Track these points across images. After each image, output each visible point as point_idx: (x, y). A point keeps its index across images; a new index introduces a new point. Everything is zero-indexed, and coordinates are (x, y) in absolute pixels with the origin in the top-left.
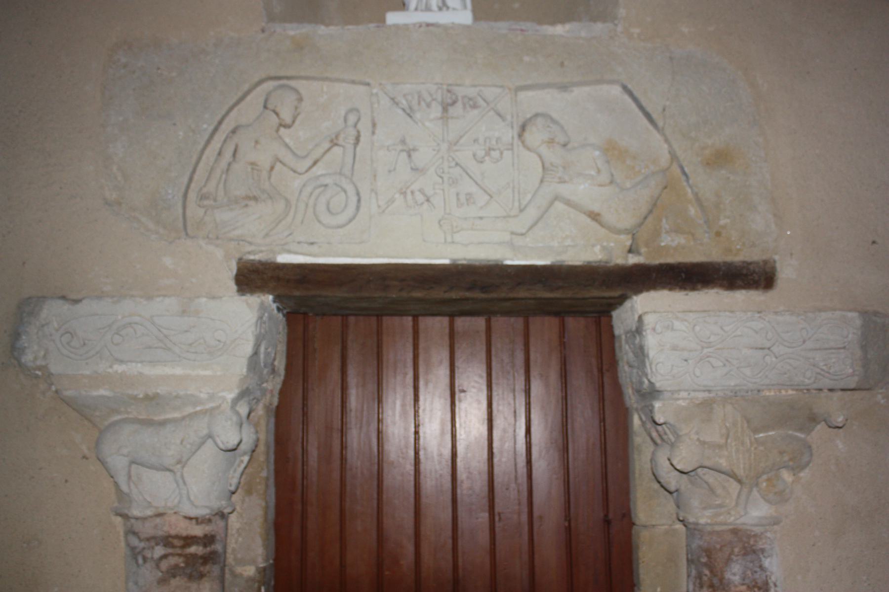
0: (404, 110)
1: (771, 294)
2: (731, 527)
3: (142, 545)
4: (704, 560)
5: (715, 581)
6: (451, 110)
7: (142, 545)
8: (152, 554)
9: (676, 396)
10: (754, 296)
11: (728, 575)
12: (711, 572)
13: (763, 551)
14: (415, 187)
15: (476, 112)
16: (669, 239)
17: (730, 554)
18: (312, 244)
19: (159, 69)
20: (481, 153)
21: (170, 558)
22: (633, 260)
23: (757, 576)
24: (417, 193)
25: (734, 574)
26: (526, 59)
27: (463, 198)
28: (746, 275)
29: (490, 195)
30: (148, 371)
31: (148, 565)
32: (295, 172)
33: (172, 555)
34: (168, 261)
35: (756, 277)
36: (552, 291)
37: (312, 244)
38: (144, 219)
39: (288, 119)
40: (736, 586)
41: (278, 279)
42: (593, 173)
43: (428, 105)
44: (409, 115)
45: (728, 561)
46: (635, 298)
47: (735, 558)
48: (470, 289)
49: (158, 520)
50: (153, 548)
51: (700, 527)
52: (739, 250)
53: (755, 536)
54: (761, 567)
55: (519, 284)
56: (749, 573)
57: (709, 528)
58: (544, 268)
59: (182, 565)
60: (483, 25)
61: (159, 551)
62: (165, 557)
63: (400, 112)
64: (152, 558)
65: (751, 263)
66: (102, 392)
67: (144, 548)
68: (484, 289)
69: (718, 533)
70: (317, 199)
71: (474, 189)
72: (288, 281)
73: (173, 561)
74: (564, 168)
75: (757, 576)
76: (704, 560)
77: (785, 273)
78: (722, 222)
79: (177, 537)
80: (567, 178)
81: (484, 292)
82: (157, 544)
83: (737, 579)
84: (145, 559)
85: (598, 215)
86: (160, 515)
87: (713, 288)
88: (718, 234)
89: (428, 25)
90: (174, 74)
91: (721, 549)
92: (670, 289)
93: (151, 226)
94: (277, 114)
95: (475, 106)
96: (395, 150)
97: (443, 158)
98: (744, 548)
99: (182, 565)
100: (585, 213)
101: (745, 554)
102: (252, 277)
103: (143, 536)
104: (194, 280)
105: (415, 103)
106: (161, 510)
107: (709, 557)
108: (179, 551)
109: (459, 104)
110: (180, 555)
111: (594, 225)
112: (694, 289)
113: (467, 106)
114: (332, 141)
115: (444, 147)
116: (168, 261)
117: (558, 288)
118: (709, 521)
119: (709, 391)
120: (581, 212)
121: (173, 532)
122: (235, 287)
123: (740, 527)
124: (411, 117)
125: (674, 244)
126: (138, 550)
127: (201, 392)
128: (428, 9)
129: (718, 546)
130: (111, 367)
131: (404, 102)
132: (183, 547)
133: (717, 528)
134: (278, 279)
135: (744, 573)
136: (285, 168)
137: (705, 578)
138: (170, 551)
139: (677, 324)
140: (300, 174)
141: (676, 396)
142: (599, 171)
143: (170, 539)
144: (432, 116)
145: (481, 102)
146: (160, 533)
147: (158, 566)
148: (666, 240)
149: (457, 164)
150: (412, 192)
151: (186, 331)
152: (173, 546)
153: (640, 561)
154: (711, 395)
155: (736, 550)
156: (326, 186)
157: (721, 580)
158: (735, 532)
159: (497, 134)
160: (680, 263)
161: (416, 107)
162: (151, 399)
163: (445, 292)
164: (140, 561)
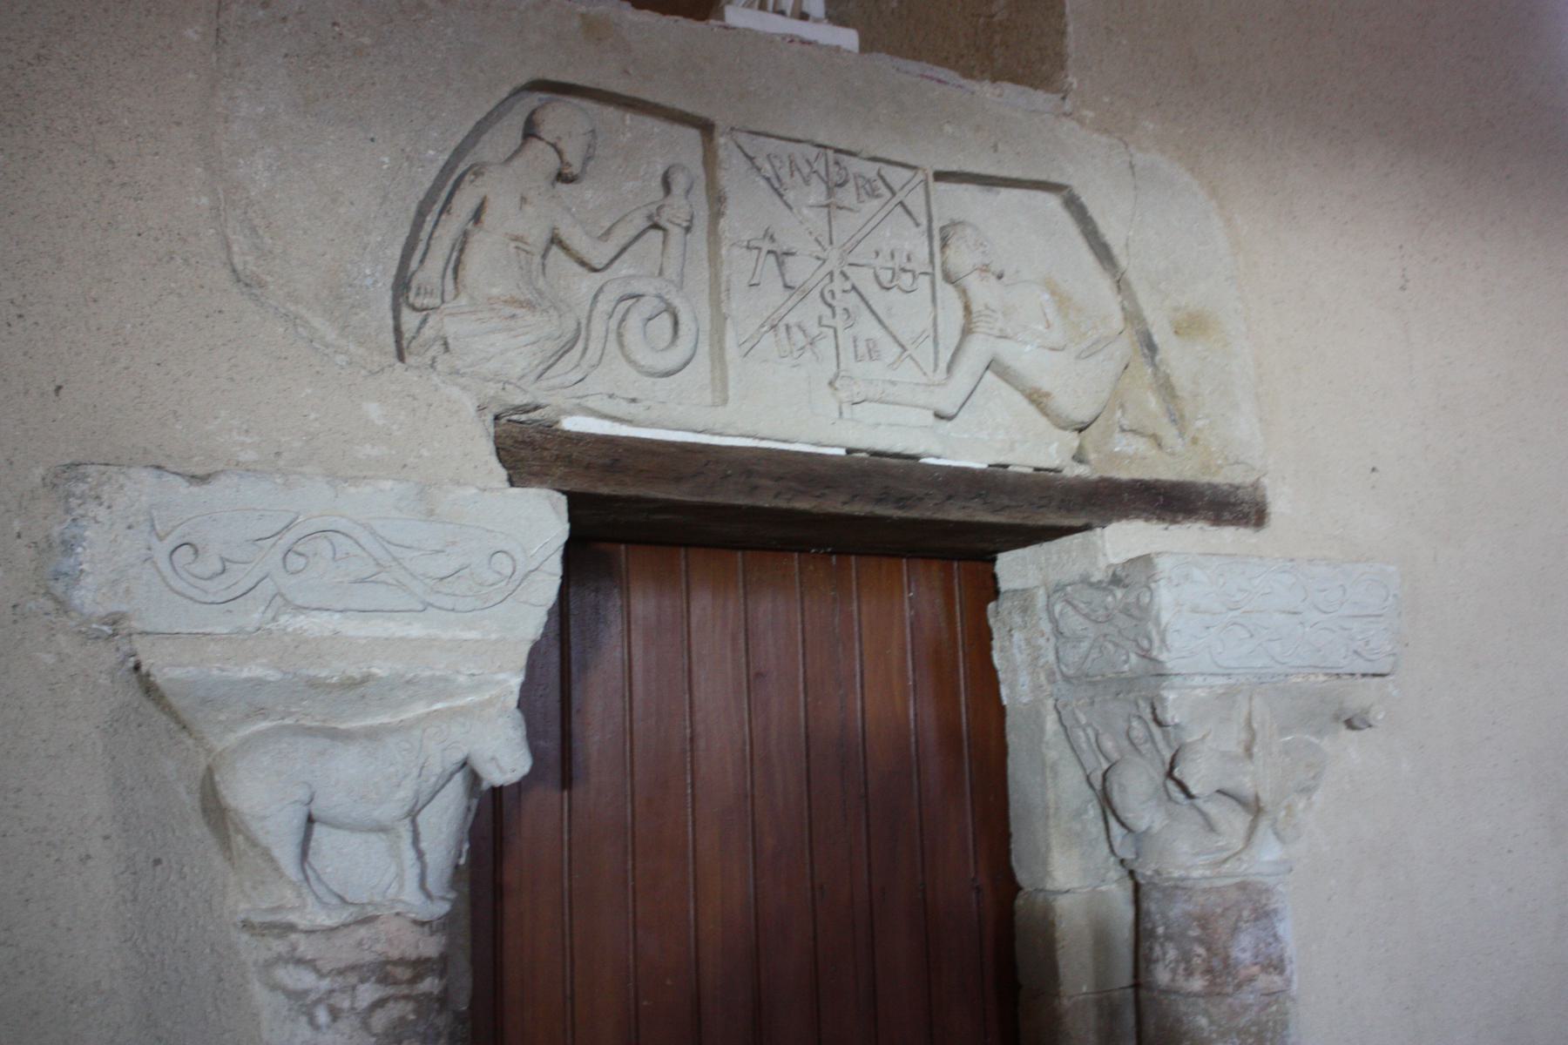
0: (768, 179)
1: (1264, 533)
2: (1238, 880)
3: (325, 984)
4: (1194, 932)
5: (1216, 963)
6: (840, 193)
7: (325, 984)
8: (354, 998)
9: (1189, 683)
10: (1229, 537)
11: (1235, 953)
12: (1208, 950)
13: (1275, 911)
14: (791, 319)
15: (876, 203)
16: (1124, 442)
17: (1237, 921)
18: (634, 400)
19: (334, 24)
20: (886, 276)
21: (391, 1004)
22: (1081, 471)
23: (1271, 950)
24: (795, 330)
25: (1244, 950)
26: (948, 129)
27: (862, 349)
28: (1234, 505)
29: (902, 346)
30: (353, 628)
31: (343, 1025)
32: (583, 263)
33: (396, 998)
34: (373, 410)
35: (1246, 508)
36: (995, 511)
37: (634, 400)
38: (317, 322)
39: (575, 169)
40: (1246, 967)
41: (569, 461)
42: (1041, 328)
43: (807, 182)
44: (776, 190)
45: (1235, 930)
46: (1098, 530)
47: (1243, 925)
48: (879, 501)
49: (363, 932)
50: (354, 988)
51: (1189, 883)
52: (1220, 467)
53: (1267, 890)
54: (1275, 936)
55: (950, 497)
56: (1262, 945)
57: (1206, 884)
58: (982, 471)
59: (412, 1017)
60: (883, 62)
61: (368, 993)
62: (380, 1004)
63: (763, 183)
64: (353, 1008)
65: (1238, 488)
66: (254, 671)
67: (331, 991)
68: (901, 502)
69: (1218, 890)
70: (623, 320)
71: (876, 332)
72: (588, 467)
73: (396, 1010)
74: (1005, 314)
75: (1271, 950)
76: (1194, 932)
77: (1279, 505)
78: (1199, 424)
79: (401, 962)
80: (1009, 331)
81: (899, 508)
82: (362, 981)
83: (1246, 957)
84: (335, 1014)
85: (1047, 395)
86: (367, 920)
87: (1197, 520)
88: (1195, 441)
89: (803, 42)
90: (366, 40)
91: (1222, 915)
92: (1147, 520)
93: (331, 335)
94: (560, 153)
95: (874, 194)
96: (759, 249)
97: (831, 274)
98: (1255, 910)
99: (412, 1017)
100: (1023, 392)
101: (1256, 919)
102: (527, 450)
103: (326, 967)
104: (425, 453)
105: (784, 172)
106: (370, 911)
107: (1203, 927)
108: (405, 990)
109: (851, 186)
110: (407, 997)
111: (1032, 410)
112: (1174, 521)
113: (862, 191)
114: (650, 217)
115: (833, 255)
116: (373, 410)
117: (1003, 508)
118: (1208, 873)
119: (1229, 675)
120: (1017, 388)
121: (395, 954)
122: (502, 473)
123: (1251, 878)
124: (781, 196)
125: (1130, 451)
126: (313, 997)
127: (458, 672)
128: (804, 16)
129: (1219, 910)
130: (274, 619)
131: (768, 166)
132: (414, 980)
133: (1219, 883)
134: (569, 461)
135: (1256, 946)
136: (930, 309)
137: (1196, 961)
138: (390, 991)
139: (1197, 573)
140: (595, 270)
141: (1189, 683)
142: (1048, 326)
143: (389, 968)
144: (812, 201)
145: (884, 190)
146: (368, 957)
147: (365, 1025)
148: (1124, 444)
149: (854, 288)
150: (788, 328)
151: (438, 552)
152: (396, 983)
153: (1059, 946)
154: (1232, 681)
155: (1245, 913)
156: (638, 297)
157: (1226, 959)
158: (1242, 887)
159: (907, 246)
160: (1157, 481)
161: (787, 179)
162: (355, 687)
163: (845, 503)
164: (322, 1016)
